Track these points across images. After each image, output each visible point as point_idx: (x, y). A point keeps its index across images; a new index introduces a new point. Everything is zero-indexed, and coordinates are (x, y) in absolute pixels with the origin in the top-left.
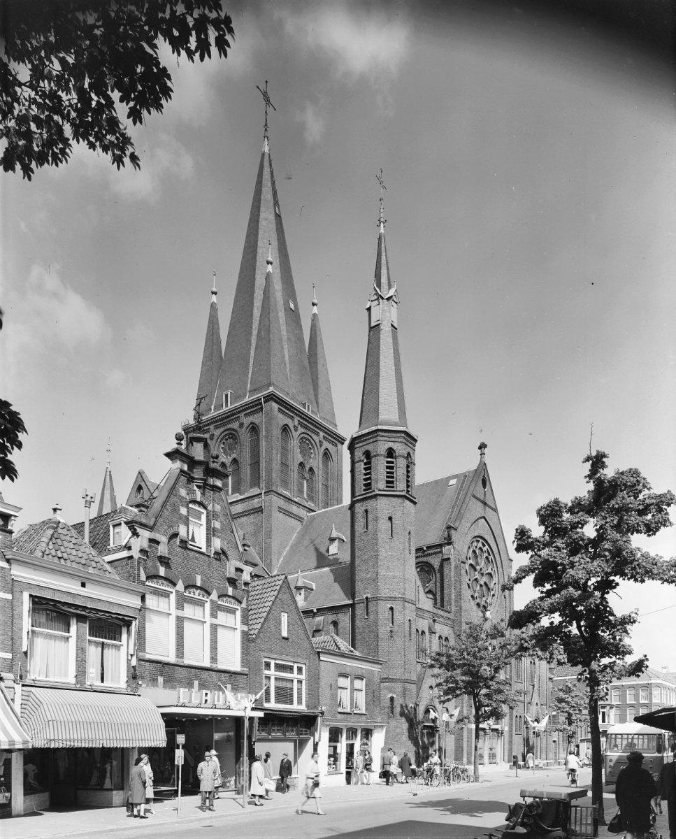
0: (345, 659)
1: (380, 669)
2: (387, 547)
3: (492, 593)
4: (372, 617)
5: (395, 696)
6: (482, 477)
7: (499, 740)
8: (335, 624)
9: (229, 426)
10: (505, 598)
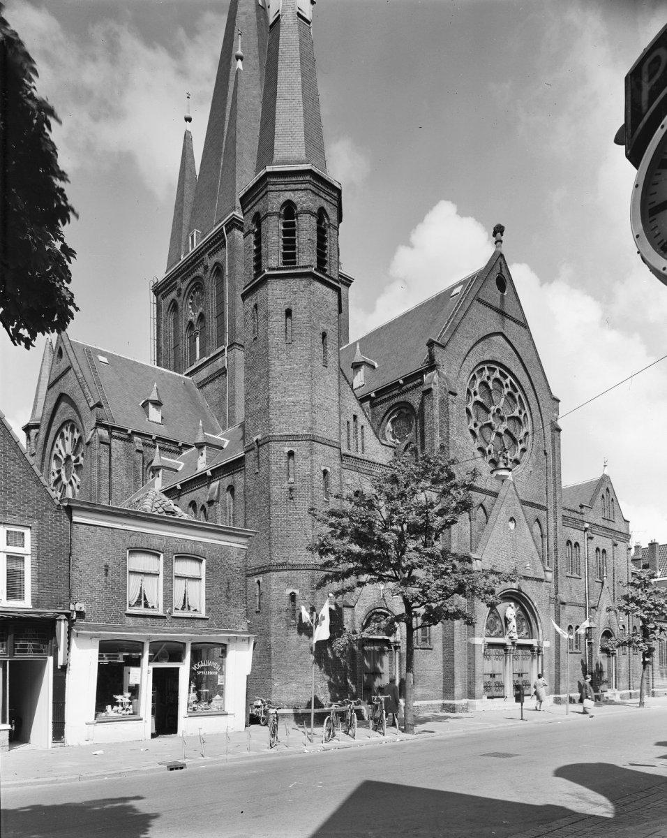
0: (186, 531)
1: (244, 544)
2: (283, 356)
3: (520, 447)
4: (263, 470)
5: (297, 592)
6: (497, 275)
7: (535, 661)
8: (231, 489)
9: (195, 274)
10: (546, 454)
